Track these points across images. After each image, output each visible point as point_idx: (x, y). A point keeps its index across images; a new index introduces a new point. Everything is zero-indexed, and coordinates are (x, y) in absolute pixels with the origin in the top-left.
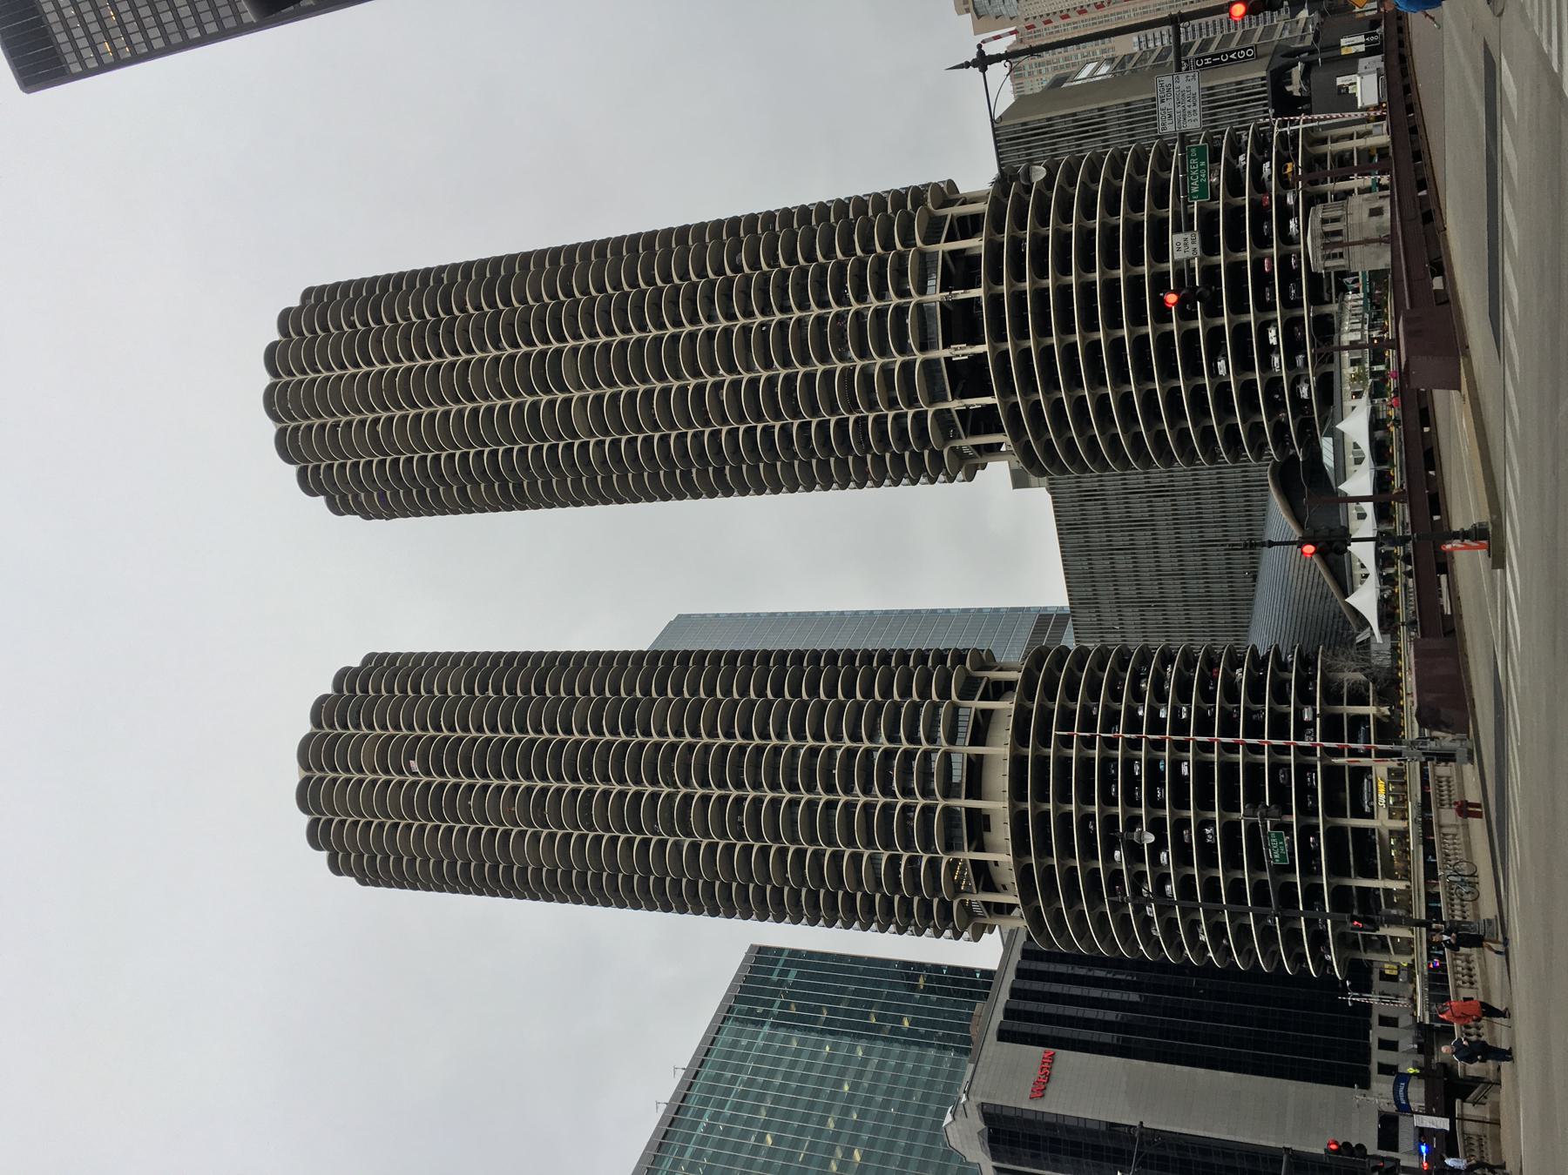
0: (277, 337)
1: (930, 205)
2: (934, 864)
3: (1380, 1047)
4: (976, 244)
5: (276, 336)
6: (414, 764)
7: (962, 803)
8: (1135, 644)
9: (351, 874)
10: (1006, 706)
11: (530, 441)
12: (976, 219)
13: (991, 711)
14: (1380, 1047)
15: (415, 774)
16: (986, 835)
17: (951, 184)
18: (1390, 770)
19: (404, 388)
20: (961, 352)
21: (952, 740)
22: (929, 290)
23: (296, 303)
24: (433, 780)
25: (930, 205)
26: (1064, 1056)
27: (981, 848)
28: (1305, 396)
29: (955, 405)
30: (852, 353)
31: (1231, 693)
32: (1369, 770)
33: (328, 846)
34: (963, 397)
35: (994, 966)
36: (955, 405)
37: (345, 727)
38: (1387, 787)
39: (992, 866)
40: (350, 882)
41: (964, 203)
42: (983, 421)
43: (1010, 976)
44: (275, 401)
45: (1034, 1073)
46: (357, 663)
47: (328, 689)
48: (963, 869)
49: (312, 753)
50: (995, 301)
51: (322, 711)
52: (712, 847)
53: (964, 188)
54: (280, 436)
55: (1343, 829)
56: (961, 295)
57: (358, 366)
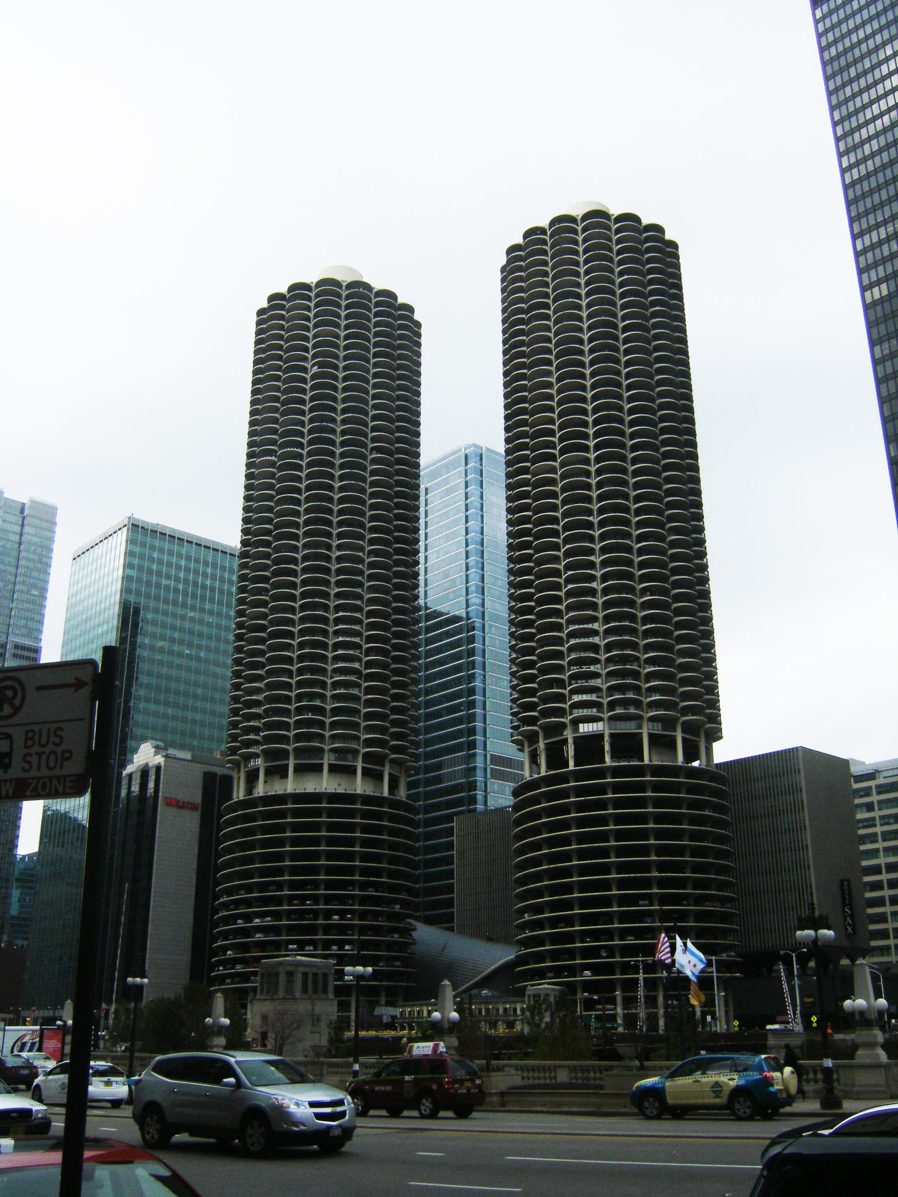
9: (509, 262)
13: (675, 748)
19: (602, 311)
22: (650, 724)
23: (668, 236)
31: (328, 914)
40: (503, 260)
42: (556, 757)
53: (716, 745)
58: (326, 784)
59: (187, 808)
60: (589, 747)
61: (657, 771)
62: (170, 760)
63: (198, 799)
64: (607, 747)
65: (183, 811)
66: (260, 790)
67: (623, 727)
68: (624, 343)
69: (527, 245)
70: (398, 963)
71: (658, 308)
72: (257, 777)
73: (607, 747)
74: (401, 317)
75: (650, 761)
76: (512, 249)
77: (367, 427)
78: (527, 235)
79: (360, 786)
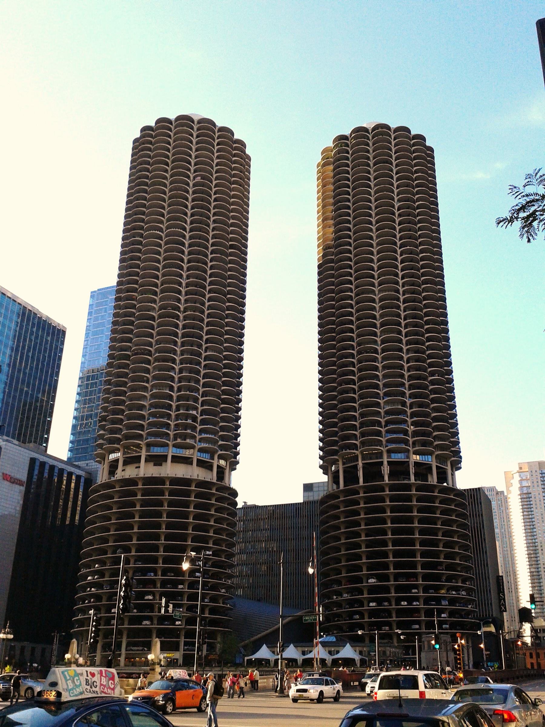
1: (453, 459)
2: (140, 437)
3: (22, 646)
4: (433, 479)
6: (198, 179)
7: (144, 454)
12: (445, 480)
14: (22, 646)
15: (194, 178)
16: (152, 464)
17: (460, 468)
18: (177, 659)
19: (381, 194)
20: (386, 470)
21: (201, 450)
23: (428, 144)
24: (185, 183)
25: (453, 459)
26: (23, 489)
27: (146, 461)
28: (143, 623)
29: (360, 463)
32: (177, 649)
35: (49, 452)
36: (360, 463)
37: (218, 144)
38: (169, 657)
39: (137, 465)
41: (452, 475)
42: (351, 476)
43: (42, 458)
44: (382, 129)
45: (18, 476)
46: (247, 151)
47: (461, 454)
48: (136, 451)
49: (207, 124)
50: (408, 487)
51: (226, 132)
53: (458, 474)
54: (365, 130)
55: (178, 636)
56: (412, 470)
57: (396, 174)
58: (171, 470)
59: (17, 484)
62: (10, 444)
63: (23, 476)
65: (14, 485)
66: (120, 474)
67: (181, 453)
68: (398, 210)
69: (158, 128)
70: (358, 617)
71: (421, 202)
72: (116, 467)
74: (236, 149)
76: (145, 129)
77: (206, 282)
78: (159, 121)
79: (195, 473)
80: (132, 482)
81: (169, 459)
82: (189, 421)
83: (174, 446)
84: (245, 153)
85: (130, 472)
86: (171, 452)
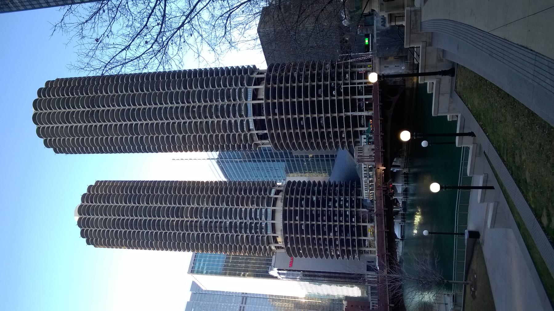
0: (37, 97)
5: (37, 97)
8: (287, 63)
10: (262, 87)
11: (111, 228)
20: (261, 132)
24: (115, 218)
30: (233, 231)
33: (87, 236)
34: (257, 130)
46: (93, 184)
52: (208, 235)
58: (279, 221)
60: (259, 125)
61: (267, 97)
64: (259, 118)
73: (259, 118)
75: (262, 99)
79: (280, 207)
80: (286, 239)
81: (273, 222)
82: (253, 225)
83: (247, 116)
84: (95, 186)
85: (280, 239)
86: (270, 222)
